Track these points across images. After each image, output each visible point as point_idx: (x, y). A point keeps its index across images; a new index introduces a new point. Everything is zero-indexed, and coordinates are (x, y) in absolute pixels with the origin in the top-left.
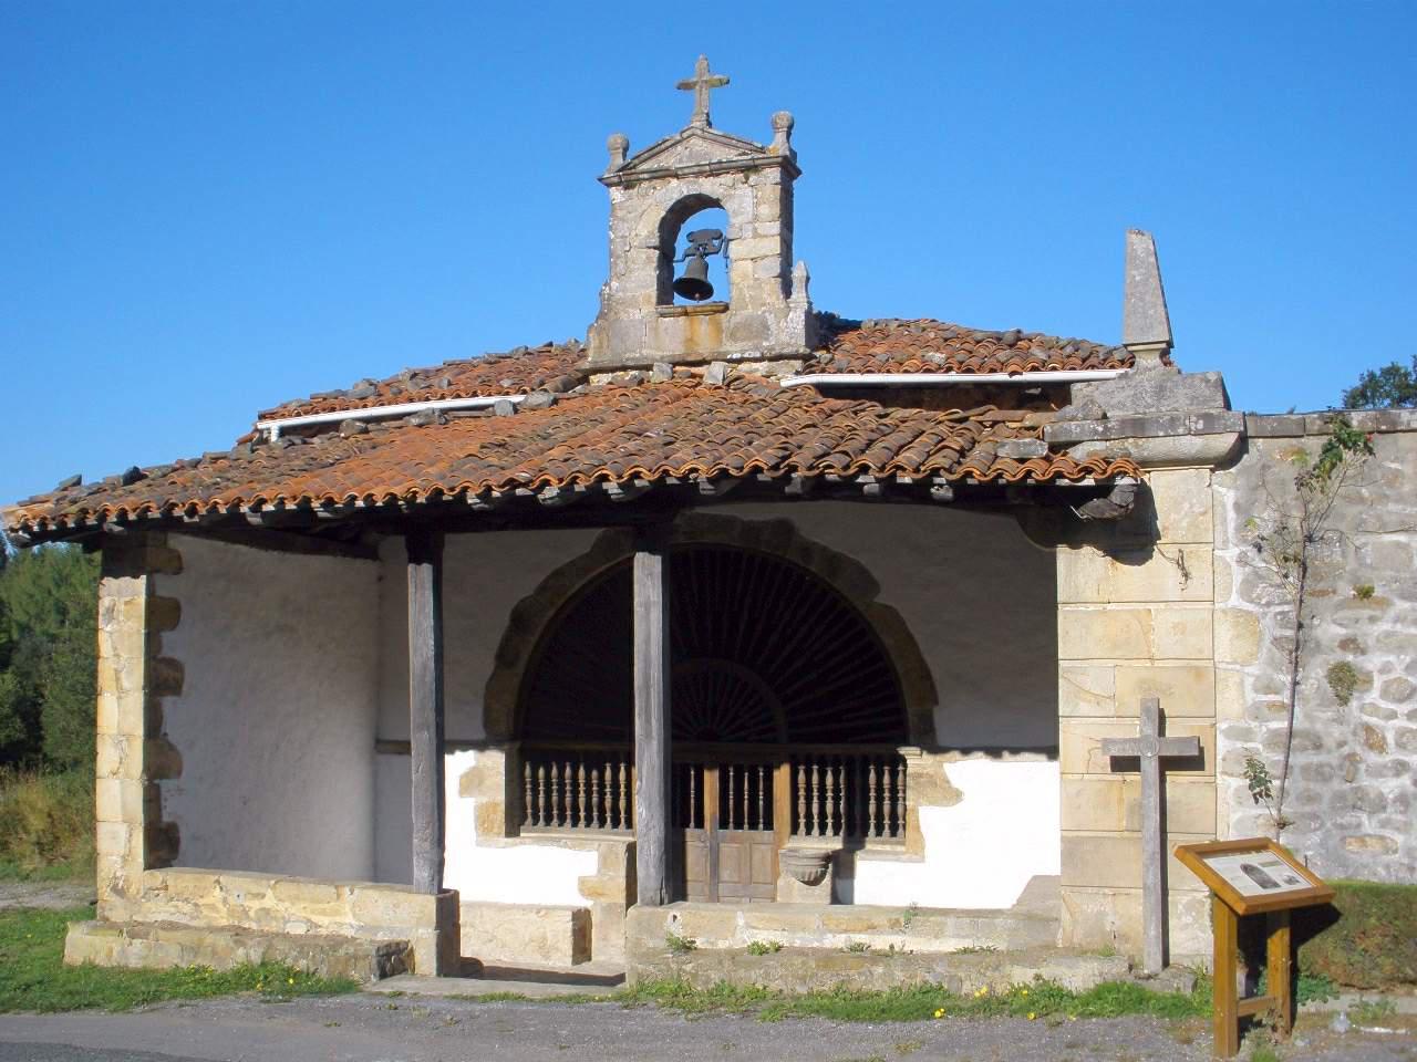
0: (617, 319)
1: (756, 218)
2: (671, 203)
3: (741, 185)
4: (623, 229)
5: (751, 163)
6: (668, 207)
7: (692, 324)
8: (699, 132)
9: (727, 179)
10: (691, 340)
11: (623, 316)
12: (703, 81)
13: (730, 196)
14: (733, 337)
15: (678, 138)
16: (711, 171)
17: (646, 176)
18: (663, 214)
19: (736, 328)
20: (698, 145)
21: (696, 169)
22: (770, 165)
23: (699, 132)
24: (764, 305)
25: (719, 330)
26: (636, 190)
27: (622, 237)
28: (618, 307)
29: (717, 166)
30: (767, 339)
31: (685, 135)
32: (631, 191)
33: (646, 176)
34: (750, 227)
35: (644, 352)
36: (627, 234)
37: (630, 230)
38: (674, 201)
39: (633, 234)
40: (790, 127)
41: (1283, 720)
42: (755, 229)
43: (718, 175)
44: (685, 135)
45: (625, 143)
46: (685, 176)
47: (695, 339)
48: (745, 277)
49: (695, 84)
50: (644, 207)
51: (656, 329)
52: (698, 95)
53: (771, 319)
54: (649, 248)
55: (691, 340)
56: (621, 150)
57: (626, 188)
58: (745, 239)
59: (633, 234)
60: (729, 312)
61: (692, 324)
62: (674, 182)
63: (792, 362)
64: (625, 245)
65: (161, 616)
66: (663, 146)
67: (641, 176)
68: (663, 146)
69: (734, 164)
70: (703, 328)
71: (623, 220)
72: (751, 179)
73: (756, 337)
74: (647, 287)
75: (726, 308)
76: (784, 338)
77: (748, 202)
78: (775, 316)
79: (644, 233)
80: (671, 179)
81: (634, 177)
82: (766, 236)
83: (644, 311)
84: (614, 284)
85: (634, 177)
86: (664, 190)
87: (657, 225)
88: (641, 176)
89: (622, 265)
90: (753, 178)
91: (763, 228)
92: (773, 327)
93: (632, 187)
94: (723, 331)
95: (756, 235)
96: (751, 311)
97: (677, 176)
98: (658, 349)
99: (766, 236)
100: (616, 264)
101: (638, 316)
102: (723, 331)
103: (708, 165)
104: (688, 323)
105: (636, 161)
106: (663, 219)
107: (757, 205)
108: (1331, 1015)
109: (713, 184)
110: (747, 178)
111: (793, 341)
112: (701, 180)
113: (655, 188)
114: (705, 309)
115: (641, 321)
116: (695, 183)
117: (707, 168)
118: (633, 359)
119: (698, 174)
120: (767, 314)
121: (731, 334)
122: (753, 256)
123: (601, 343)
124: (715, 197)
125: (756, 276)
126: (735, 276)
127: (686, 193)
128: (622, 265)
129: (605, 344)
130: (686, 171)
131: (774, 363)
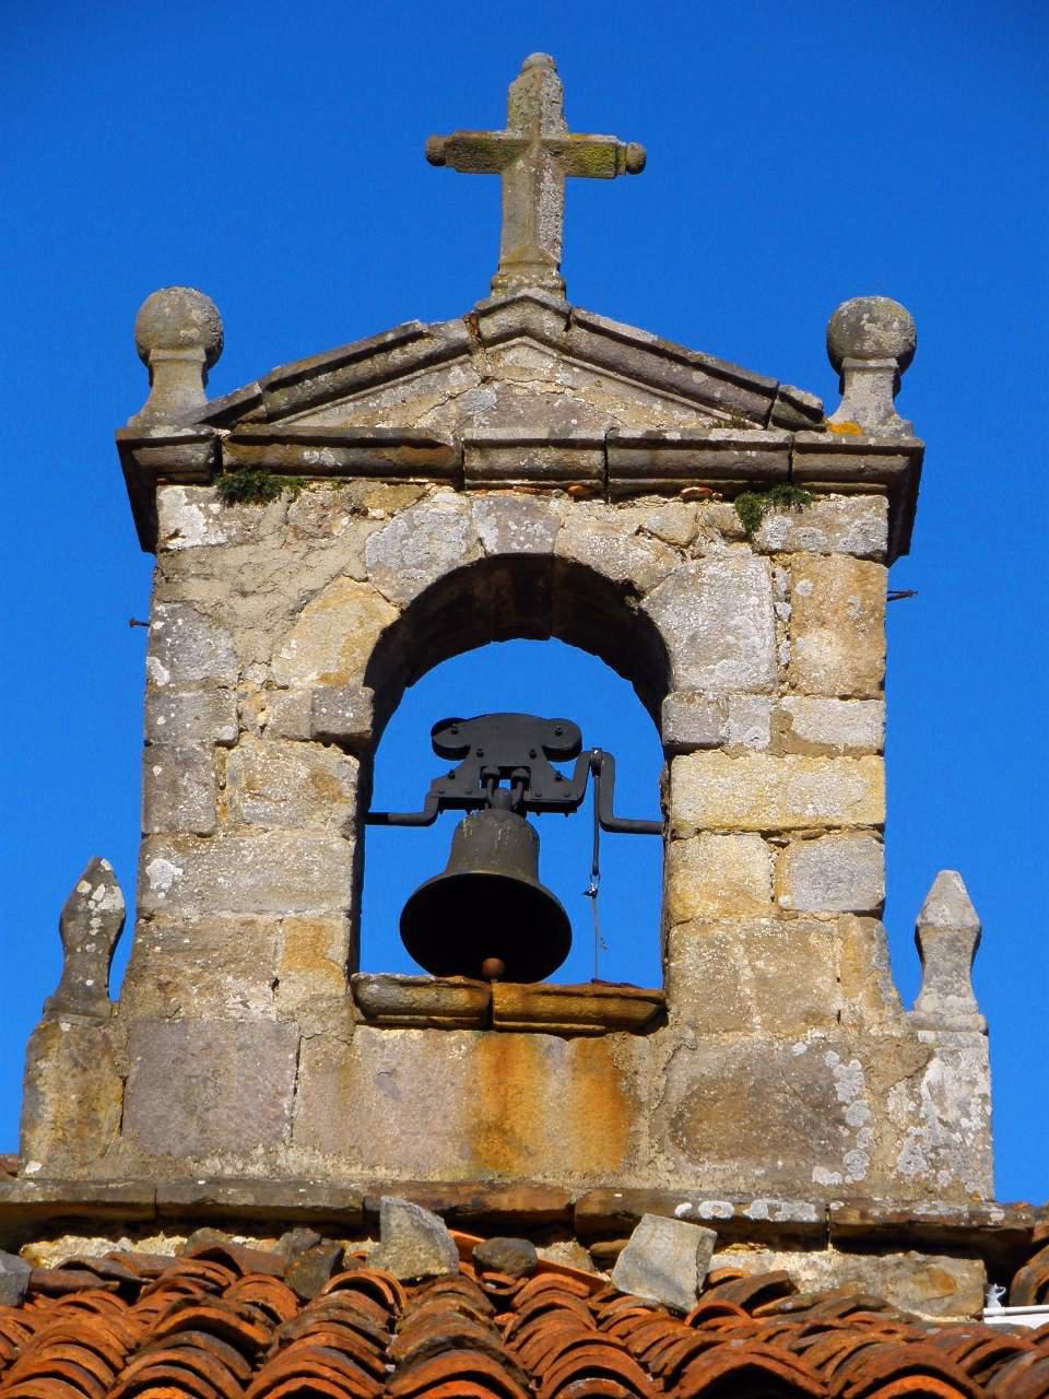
0: (166, 1016)
1: (786, 678)
2: (429, 578)
3: (719, 545)
4: (210, 652)
5: (778, 461)
6: (414, 592)
7: (501, 1066)
8: (550, 324)
9: (650, 511)
10: (498, 1128)
11: (197, 1004)
12: (546, 144)
13: (683, 581)
14: (682, 1131)
15: (459, 332)
16: (608, 471)
17: (329, 456)
18: (391, 615)
19: (696, 1096)
20: (532, 370)
21: (544, 458)
22: (849, 483)
23: (550, 324)
24: (814, 1017)
25: (622, 1100)
26: (276, 508)
27: (206, 684)
28: (178, 962)
29: (639, 457)
30: (833, 1159)
31: (489, 327)
32: (254, 510)
33: (329, 456)
34: (762, 708)
35: (294, 1160)
36: (230, 675)
37: (244, 660)
38: (441, 569)
39: (257, 675)
40: (905, 359)
41: (497, 545)
42: (783, 720)
43: (622, 497)
44: (489, 327)
45: (496, 792)
46: (491, 479)
47: (518, 1123)
48: (739, 894)
49: (513, 150)
50: (309, 581)
51: (342, 1070)
52: (524, 195)
53: (848, 1079)
54: (325, 739)
55: (498, 1128)
56: (199, 354)
57: (231, 497)
58: (740, 750)
59: (257, 675)
60: (663, 1032)
61: (501, 1066)
62: (444, 498)
63: (943, 1263)
64: (219, 716)
65: (160, 347)
66: (397, 357)
67: (310, 455)
68: (397, 357)
69: (707, 458)
70: (553, 1086)
71: (213, 618)
72: (768, 525)
73: (781, 1145)
74: (311, 897)
75: (656, 1018)
76: (906, 1160)
77: (754, 621)
78: (868, 1070)
79: (305, 679)
80: (431, 486)
81: (274, 454)
82: (829, 751)
83: (294, 992)
84: (163, 869)
85: (274, 454)
86: (400, 523)
87: (362, 656)
88: (310, 455)
89: (199, 796)
90: (775, 525)
91: (820, 718)
92: (858, 1113)
93: (263, 495)
94: (639, 1106)
95: (785, 741)
96: (759, 1035)
97: (457, 479)
98: (356, 1153)
99: (829, 751)
100: (174, 787)
101: (262, 1006)
102: (639, 1106)
103: (602, 446)
104: (484, 1059)
105: (281, 399)
106: (388, 633)
107: (789, 628)
108: (762, 980)
109: (609, 528)
110: (753, 520)
111: (944, 1177)
112: (558, 505)
113: (359, 512)
114: (575, 1005)
115: (278, 1033)
116: (532, 511)
117: (596, 457)
118: (241, 1181)
119: (544, 481)
120: (832, 1057)
121: (676, 1122)
122: (772, 820)
123: (87, 1101)
124: (614, 573)
125: (784, 900)
126: (694, 891)
127: (492, 547)
128: (199, 796)
129: (108, 1113)
130: (504, 459)
131: (864, 1262)
